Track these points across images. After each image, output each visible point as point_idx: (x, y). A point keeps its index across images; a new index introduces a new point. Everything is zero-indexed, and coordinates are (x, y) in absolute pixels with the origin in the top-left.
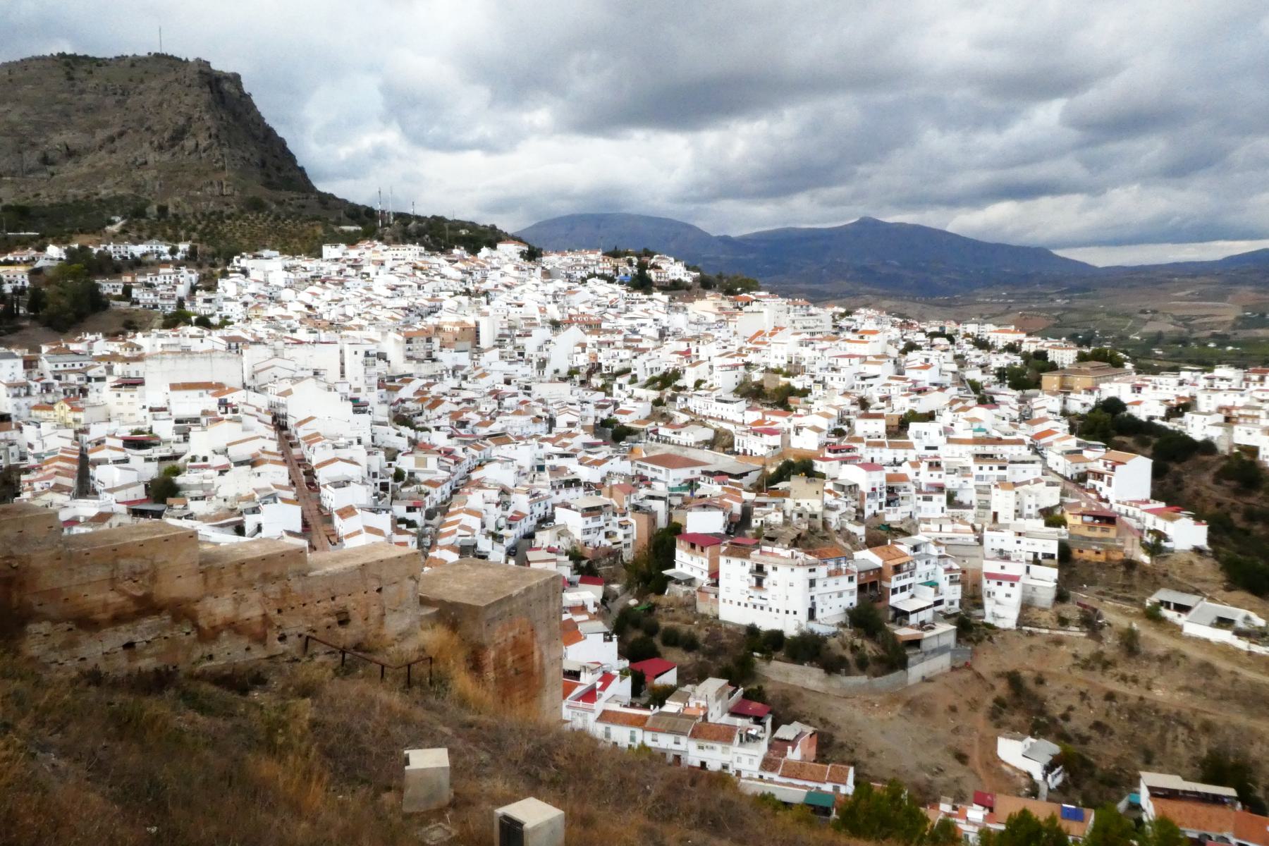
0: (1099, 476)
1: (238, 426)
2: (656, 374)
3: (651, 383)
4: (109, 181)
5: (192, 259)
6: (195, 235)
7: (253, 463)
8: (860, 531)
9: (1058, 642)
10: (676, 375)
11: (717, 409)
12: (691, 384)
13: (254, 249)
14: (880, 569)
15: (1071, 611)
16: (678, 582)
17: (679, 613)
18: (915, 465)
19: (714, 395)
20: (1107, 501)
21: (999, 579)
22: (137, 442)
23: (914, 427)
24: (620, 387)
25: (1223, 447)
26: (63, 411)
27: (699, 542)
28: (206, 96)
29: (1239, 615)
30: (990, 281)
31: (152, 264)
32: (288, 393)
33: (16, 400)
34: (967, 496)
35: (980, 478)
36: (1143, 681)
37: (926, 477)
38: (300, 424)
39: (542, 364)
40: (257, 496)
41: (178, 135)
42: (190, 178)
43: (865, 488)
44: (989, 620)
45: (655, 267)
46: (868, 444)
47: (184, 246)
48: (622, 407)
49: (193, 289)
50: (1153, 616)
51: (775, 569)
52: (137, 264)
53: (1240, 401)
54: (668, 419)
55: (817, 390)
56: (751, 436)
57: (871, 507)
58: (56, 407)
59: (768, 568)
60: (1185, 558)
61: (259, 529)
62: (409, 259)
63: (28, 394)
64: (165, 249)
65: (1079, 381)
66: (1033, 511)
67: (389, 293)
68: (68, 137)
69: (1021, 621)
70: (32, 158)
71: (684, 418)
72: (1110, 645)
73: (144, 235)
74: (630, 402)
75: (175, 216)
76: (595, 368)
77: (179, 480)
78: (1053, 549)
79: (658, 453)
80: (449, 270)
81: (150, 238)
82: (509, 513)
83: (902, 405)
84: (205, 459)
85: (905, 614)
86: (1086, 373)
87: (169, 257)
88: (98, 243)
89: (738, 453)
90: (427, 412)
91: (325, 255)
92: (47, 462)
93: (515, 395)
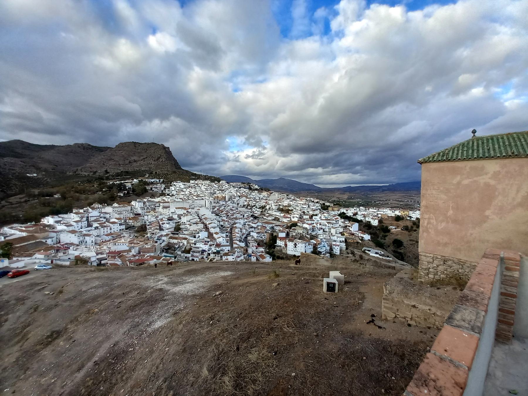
0: (350, 226)
1: (192, 216)
2: (260, 206)
3: (259, 208)
4: (144, 167)
5: (163, 182)
6: (163, 178)
7: (197, 224)
8: (309, 236)
9: (348, 257)
10: (265, 207)
11: (274, 213)
12: (268, 209)
13: (176, 180)
14: (316, 244)
15: (349, 251)
16: (277, 246)
17: (279, 253)
18: (316, 224)
19: (274, 211)
20: (351, 231)
21: (336, 245)
22: (170, 219)
23: (314, 217)
24: (254, 209)
25: (364, 221)
26: (152, 213)
27: (281, 239)
28: (164, 151)
29: (379, 252)
30: (304, 190)
31: (155, 183)
32: (199, 210)
33: (142, 211)
34: (327, 230)
35: (328, 226)
36: (365, 264)
37: (319, 226)
38: (202, 216)
39: (238, 204)
40: (198, 230)
41: (159, 158)
42: (161, 167)
43: (309, 228)
44: (334, 253)
45: (252, 186)
46: (306, 220)
47: (161, 180)
48: (255, 212)
49: (165, 189)
50: (364, 252)
51: (299, 244)
52: (152, 183)
53: (366, 213)
54: (264, 215)
55: (295, 210)
56: (283, 219)
57: (310, 232)
58: (151, 212)
59: (297, 244)
60: (367, 241)
61: (199, 237)
62: (207, 183)
63: (144, 210)
64: (158, 180)
65: (335, 209)
66: (338, 233)
67: (205, 190)
68: (135, 158)
69: (340, 253)
70: (127, 162)
71: (267, 215)
72: (357, 257)
73: (153, 177)
74: (256, 212)
75: (158, 174)
76: (249, 205)
77: (181, 227)
78: (344, 240)
79: (264, 222)
80: (215, 186)
81: (154, 178)
82: (242, 233)
83: (311, 213)
84: (185, 223)
85: (321, 252)
86: (336, 207)
87: (159, 182)
88: (144, 179)
89: (280, 222)
90: (221, 213)
91: (191, 182)
92: (153, 223)
93: (235, 210)
